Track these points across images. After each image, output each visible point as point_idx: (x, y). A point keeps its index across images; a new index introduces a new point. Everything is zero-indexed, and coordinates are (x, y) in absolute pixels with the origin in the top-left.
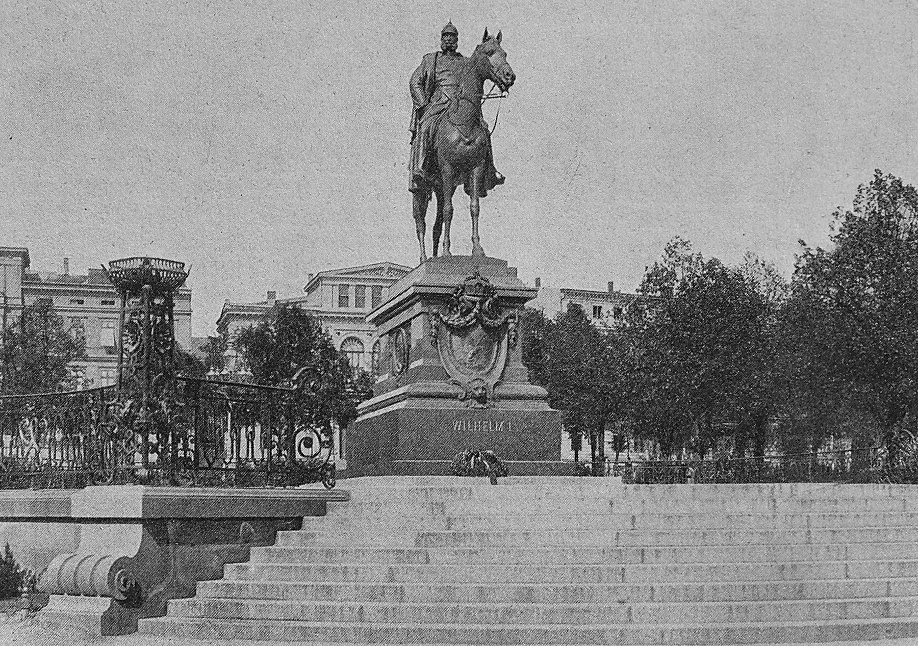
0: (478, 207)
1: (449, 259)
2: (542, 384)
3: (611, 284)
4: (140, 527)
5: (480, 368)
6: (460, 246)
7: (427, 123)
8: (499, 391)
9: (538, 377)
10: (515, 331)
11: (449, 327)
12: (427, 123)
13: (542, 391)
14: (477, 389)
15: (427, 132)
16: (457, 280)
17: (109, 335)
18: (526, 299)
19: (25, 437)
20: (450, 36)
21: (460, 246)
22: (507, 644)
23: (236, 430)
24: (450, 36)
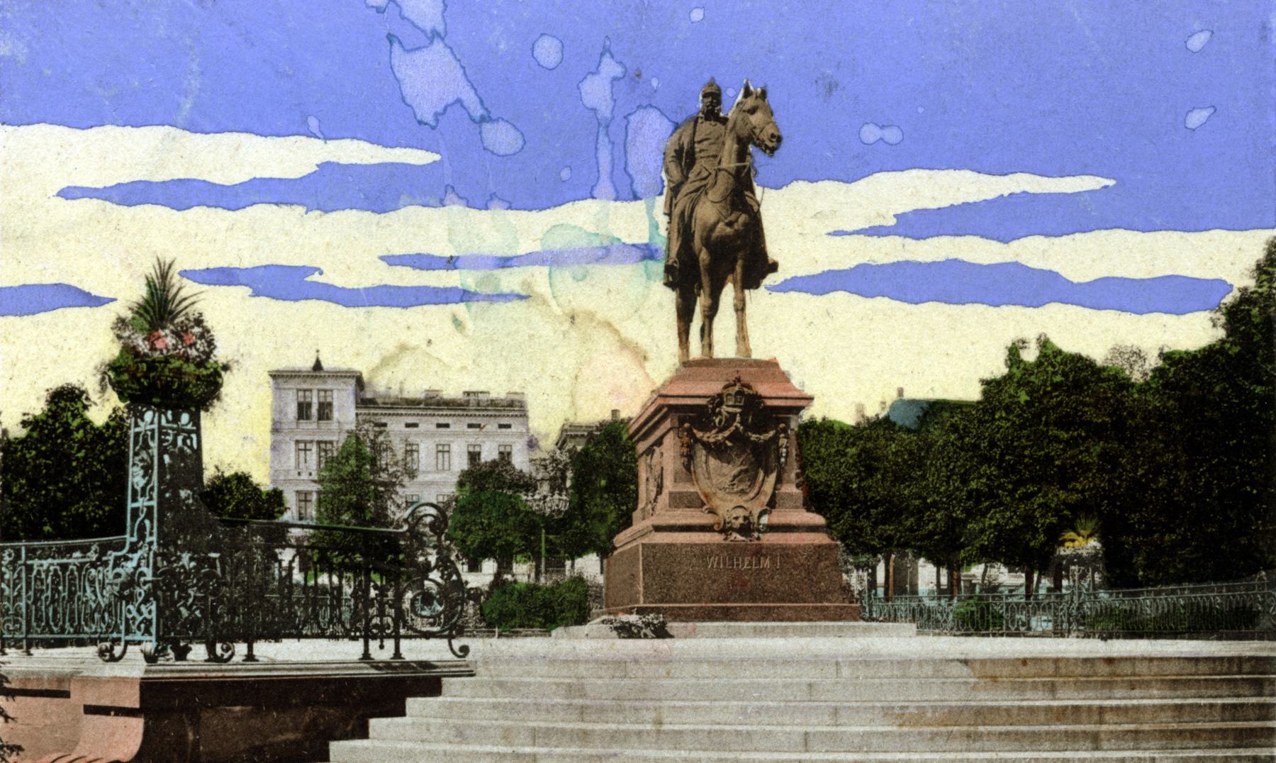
0: (743, 301)
1: (709, 363)
2: (819, 511)
3: (901, 392)
4: (255, 645)
5: (743, 492)
6: (725, 346)
7: (682, 202)
8: (765, 520)
9: (814, 501)
10: (786, 447)
11: (706, 446)
12: (682, 202)
13: (818, 519)
14: (736, 518)
15: (683, 213)
16: (715, 388)
17: (179, 118)
18: (800, 408)
19: (21, 624)
20: (714, 97)
21: (725, 346)
22: (5, 471)
23: (1169, 611)
24: (714, 97)
